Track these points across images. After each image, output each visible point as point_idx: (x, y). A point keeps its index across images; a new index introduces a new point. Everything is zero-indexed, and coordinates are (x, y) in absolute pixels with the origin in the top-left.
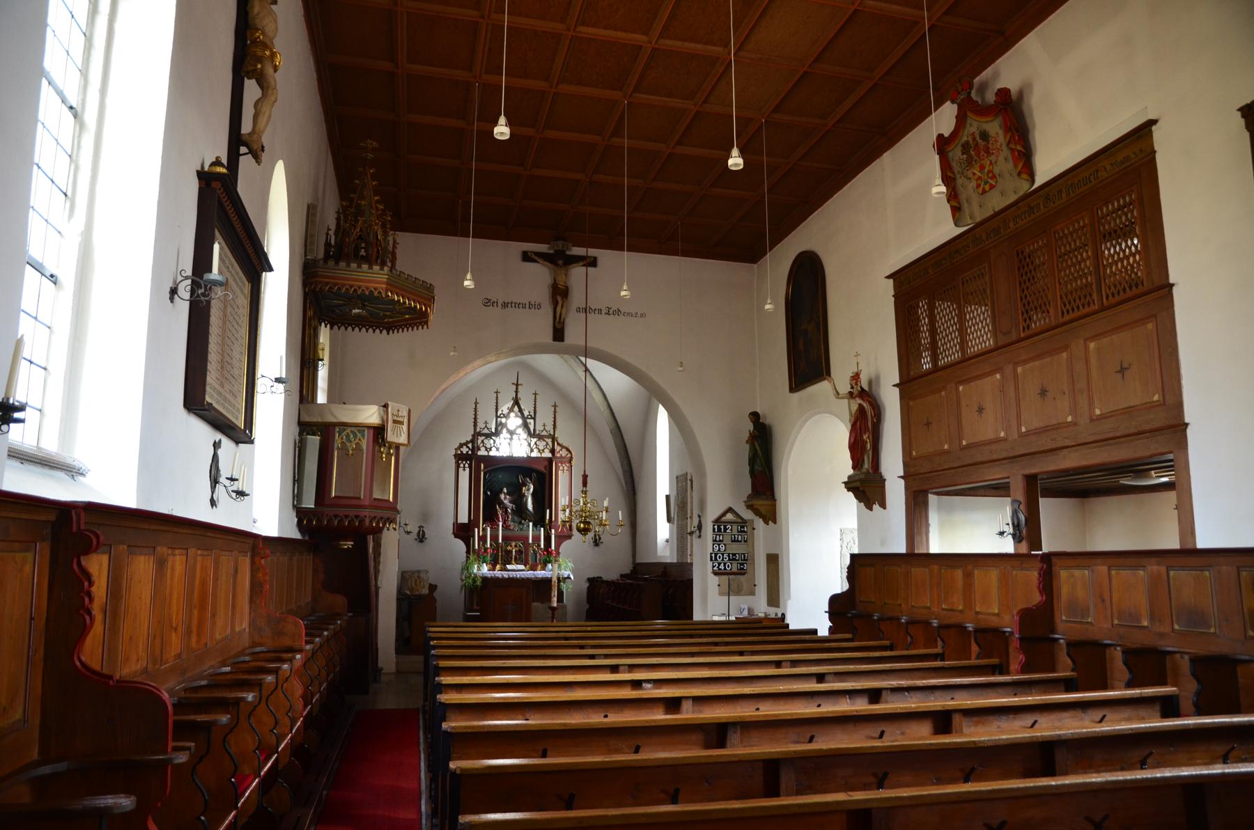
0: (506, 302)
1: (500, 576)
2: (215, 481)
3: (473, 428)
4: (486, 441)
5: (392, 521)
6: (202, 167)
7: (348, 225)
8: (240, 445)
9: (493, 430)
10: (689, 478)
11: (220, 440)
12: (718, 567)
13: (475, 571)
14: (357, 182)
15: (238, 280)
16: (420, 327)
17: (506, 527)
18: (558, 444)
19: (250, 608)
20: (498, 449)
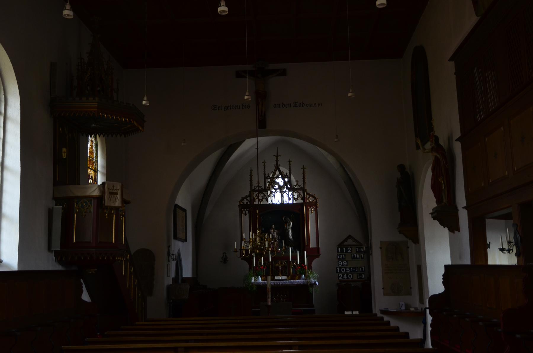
12: (342, 277)
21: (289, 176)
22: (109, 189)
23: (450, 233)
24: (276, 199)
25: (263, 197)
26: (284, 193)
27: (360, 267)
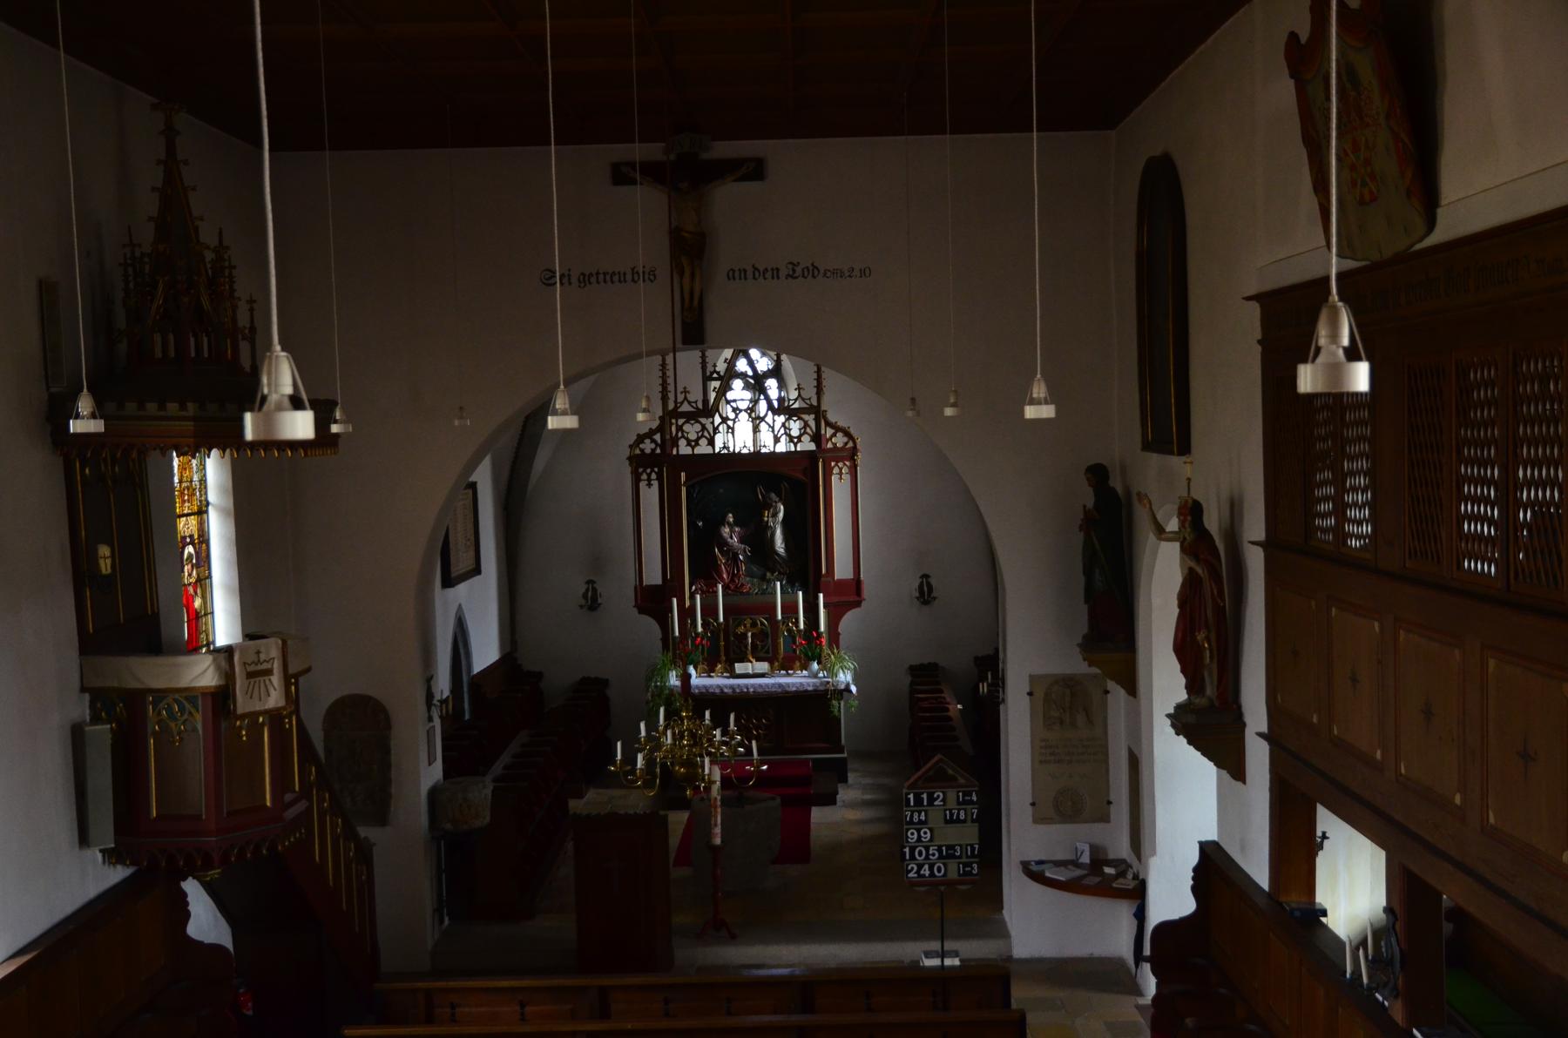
3: (660, 402)
18: (828, 424)
23: (1221, 770)
24: (739, 438)
25: (700, 434)
26: (760, 423)
27: (967, 845)
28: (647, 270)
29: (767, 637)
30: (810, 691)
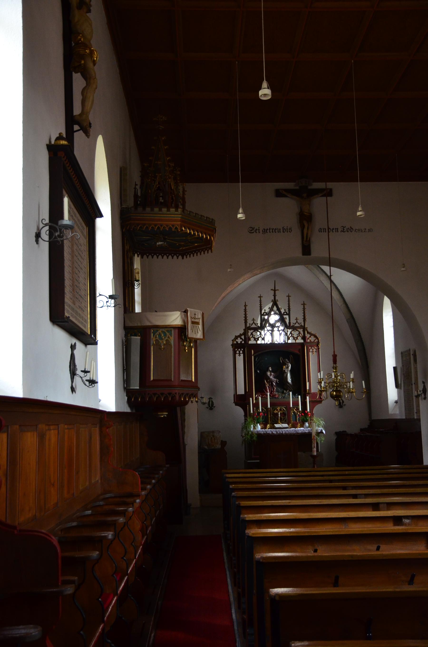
0: (266, 229)
1: (270, 433)
2: (73, 373)
3: (244, 324)
4: (254, 333)
5: (195, 396)
6: (50, 141)
7: (149, 180)
8: (88, 346)
9: (259, 325)
10: (412, 353)
11: (75, 344)
13: (252, 429)
14: (153, 147)
15: (79, 225)
16: (188, 255)
17: (272, 396)
18: (308, 332)
19: (101, 465)
20: (263, 339)
21: (288, 313)
22: (191, 317)
28: (288, 228)
29: (286, 416)
30: (307, 433)
